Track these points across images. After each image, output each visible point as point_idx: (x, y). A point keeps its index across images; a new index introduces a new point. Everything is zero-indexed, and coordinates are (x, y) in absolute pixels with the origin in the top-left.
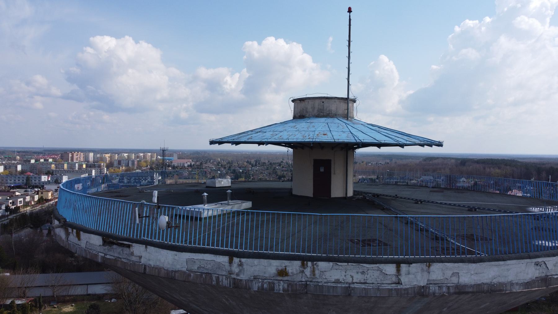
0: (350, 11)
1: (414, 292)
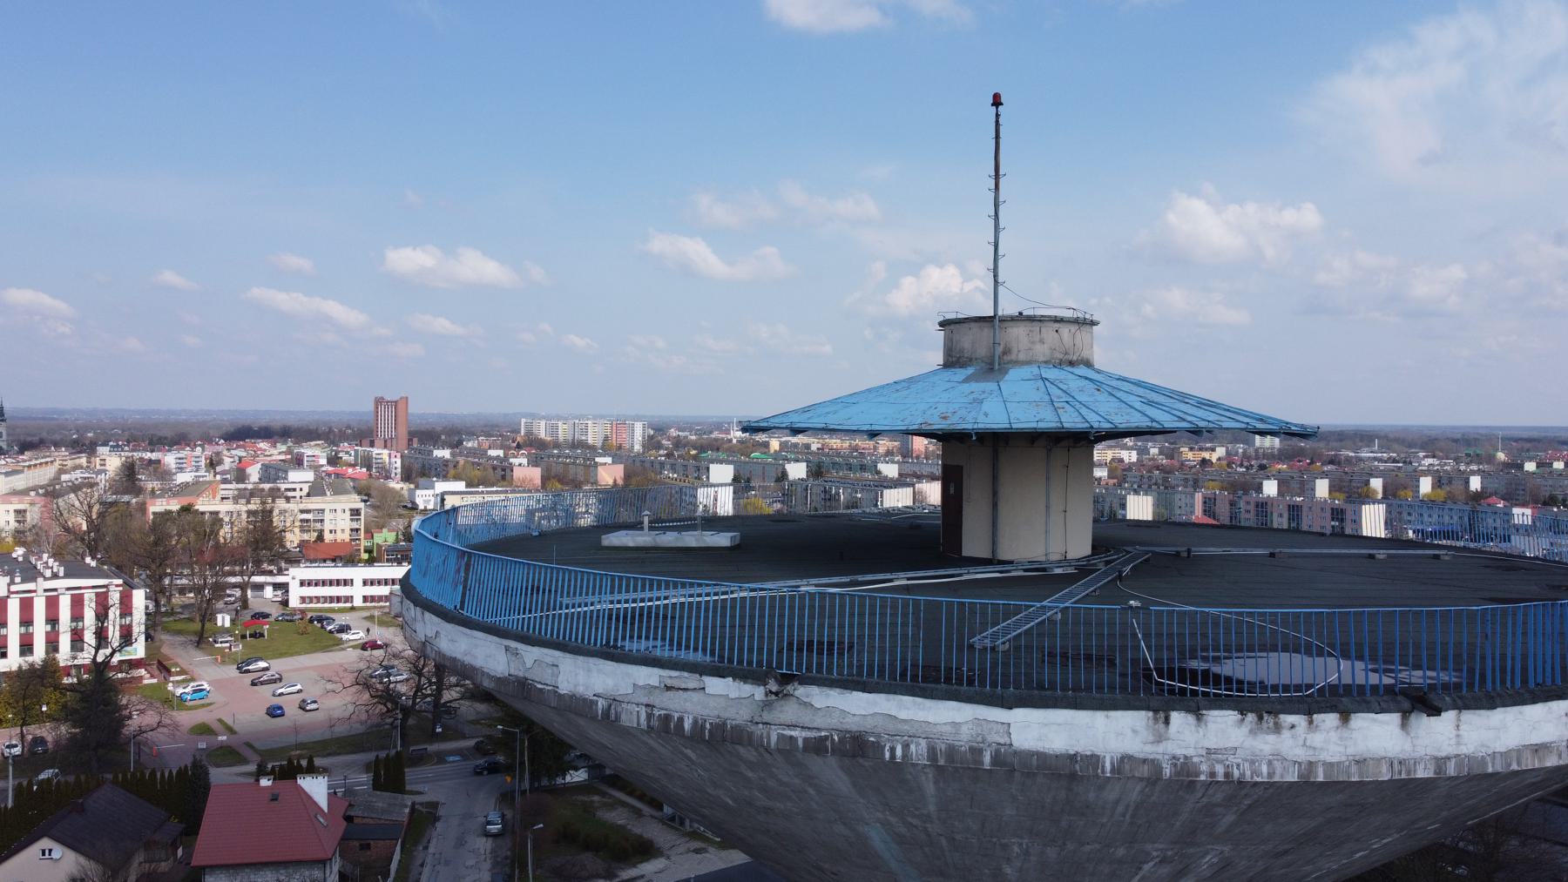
0: (997, 101)
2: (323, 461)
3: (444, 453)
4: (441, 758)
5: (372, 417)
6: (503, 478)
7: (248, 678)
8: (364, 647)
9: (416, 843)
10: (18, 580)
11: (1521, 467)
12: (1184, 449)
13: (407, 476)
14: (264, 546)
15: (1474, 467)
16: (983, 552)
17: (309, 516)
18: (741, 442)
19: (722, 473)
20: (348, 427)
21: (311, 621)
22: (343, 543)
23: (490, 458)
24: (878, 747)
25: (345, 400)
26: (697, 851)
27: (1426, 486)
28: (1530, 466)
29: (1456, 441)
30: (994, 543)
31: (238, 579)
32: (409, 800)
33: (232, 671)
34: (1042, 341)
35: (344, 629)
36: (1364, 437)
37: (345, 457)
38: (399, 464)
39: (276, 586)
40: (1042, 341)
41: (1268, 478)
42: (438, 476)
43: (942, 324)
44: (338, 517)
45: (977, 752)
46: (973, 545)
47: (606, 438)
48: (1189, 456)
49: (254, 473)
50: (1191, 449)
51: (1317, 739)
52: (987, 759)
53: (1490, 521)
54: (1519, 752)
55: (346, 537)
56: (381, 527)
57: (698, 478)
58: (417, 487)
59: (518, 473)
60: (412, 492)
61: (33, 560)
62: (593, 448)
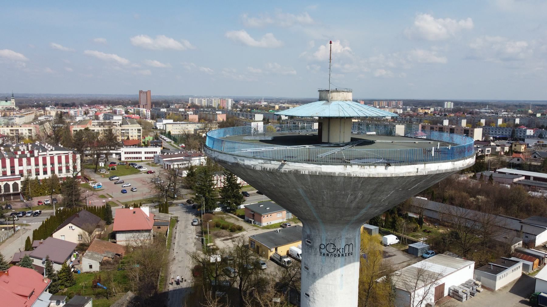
0: (331, 43)
1: (318, 230)
2: (124, 113)
3: (164, 110)
4: (177, 205)
5: (139, 96)
6: (186, 118)
7: (113, 182)
8: (148, 173)
9: (173, 227)
10: (41, 151)
11: (536, 115)
12: (419, 109)
13: (152, 118)
14: (111, 141)
15: (519, 115)
16: (326, 141)
17: (123, 131)
18: (265, 106)
19: (259, 117)
20: (130, 100)
21: (129, 165)
22: (135, 140)
23: (180, 112)
24: (300, 172)
25: (132, 92)
26: (255, 230)
27: (500, 122)
28: (539, 115)
29: (516, 106)
30: (329, 139)
31: (105, 152)
32: (170, 215)
33: (107, 180)
35: (140, 167)
36: (483, 104)
37: (131, 111)
38: (150, 114)
39: (116, 154)
41: (446, 119)
42: (163, 118)
43: (319, 91)
44: (133, 131)
45: (316, 172)
46: (324, 139)
47: (219, 105)
48: (421, 111)
49: (101, 116)
50: (422, 109)
51: (371, 170)
53: (519, 134)
54: (406, 173)
55: (136, 138)
56: (147, 135)
57: (251, 119)
58: (157, 122)
59: (191, 117)
60: (155, 124)
61: (43, 145)
62: (214, 108)
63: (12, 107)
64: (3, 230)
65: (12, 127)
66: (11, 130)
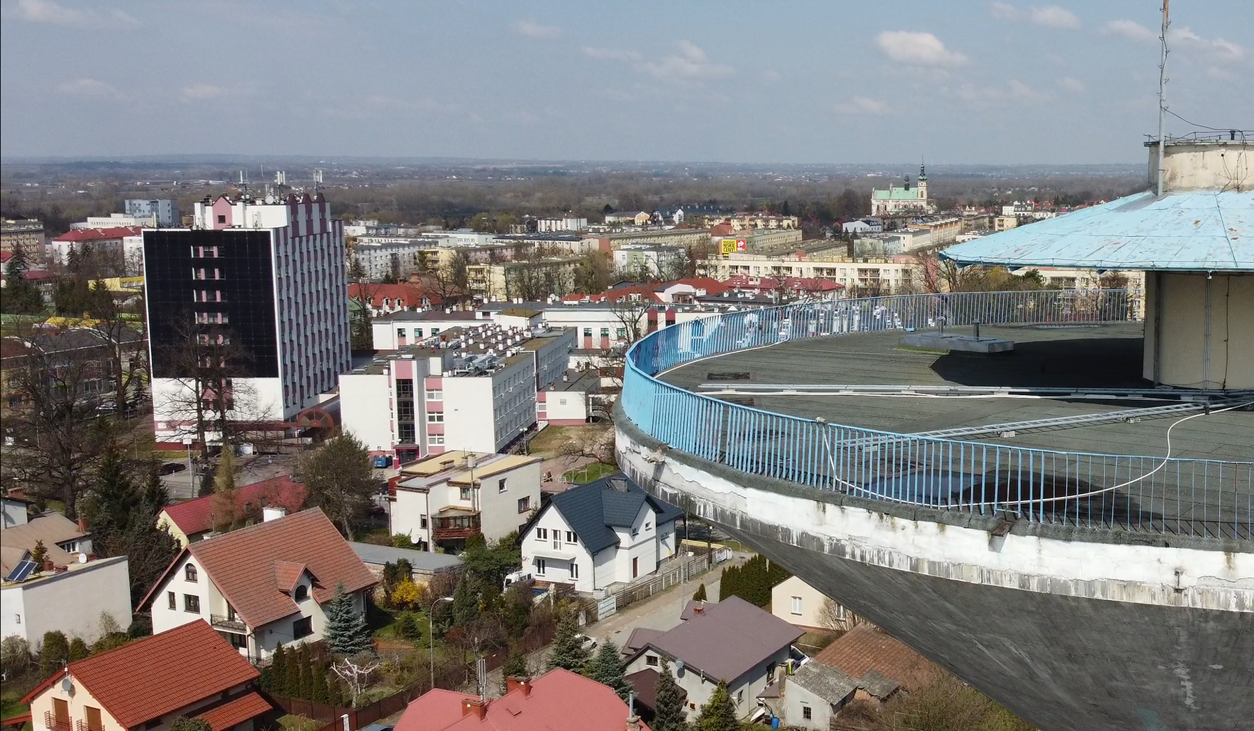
34: (1204, 167)
40: (1204, 167)
43: (1146, 144)
51: (922, 540)
52: (827, 549)
63: (919, 204)
64: (691, 554)
65: (866, 261)
66: (861, 271)
